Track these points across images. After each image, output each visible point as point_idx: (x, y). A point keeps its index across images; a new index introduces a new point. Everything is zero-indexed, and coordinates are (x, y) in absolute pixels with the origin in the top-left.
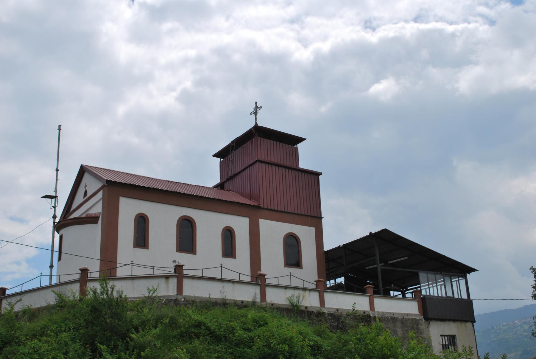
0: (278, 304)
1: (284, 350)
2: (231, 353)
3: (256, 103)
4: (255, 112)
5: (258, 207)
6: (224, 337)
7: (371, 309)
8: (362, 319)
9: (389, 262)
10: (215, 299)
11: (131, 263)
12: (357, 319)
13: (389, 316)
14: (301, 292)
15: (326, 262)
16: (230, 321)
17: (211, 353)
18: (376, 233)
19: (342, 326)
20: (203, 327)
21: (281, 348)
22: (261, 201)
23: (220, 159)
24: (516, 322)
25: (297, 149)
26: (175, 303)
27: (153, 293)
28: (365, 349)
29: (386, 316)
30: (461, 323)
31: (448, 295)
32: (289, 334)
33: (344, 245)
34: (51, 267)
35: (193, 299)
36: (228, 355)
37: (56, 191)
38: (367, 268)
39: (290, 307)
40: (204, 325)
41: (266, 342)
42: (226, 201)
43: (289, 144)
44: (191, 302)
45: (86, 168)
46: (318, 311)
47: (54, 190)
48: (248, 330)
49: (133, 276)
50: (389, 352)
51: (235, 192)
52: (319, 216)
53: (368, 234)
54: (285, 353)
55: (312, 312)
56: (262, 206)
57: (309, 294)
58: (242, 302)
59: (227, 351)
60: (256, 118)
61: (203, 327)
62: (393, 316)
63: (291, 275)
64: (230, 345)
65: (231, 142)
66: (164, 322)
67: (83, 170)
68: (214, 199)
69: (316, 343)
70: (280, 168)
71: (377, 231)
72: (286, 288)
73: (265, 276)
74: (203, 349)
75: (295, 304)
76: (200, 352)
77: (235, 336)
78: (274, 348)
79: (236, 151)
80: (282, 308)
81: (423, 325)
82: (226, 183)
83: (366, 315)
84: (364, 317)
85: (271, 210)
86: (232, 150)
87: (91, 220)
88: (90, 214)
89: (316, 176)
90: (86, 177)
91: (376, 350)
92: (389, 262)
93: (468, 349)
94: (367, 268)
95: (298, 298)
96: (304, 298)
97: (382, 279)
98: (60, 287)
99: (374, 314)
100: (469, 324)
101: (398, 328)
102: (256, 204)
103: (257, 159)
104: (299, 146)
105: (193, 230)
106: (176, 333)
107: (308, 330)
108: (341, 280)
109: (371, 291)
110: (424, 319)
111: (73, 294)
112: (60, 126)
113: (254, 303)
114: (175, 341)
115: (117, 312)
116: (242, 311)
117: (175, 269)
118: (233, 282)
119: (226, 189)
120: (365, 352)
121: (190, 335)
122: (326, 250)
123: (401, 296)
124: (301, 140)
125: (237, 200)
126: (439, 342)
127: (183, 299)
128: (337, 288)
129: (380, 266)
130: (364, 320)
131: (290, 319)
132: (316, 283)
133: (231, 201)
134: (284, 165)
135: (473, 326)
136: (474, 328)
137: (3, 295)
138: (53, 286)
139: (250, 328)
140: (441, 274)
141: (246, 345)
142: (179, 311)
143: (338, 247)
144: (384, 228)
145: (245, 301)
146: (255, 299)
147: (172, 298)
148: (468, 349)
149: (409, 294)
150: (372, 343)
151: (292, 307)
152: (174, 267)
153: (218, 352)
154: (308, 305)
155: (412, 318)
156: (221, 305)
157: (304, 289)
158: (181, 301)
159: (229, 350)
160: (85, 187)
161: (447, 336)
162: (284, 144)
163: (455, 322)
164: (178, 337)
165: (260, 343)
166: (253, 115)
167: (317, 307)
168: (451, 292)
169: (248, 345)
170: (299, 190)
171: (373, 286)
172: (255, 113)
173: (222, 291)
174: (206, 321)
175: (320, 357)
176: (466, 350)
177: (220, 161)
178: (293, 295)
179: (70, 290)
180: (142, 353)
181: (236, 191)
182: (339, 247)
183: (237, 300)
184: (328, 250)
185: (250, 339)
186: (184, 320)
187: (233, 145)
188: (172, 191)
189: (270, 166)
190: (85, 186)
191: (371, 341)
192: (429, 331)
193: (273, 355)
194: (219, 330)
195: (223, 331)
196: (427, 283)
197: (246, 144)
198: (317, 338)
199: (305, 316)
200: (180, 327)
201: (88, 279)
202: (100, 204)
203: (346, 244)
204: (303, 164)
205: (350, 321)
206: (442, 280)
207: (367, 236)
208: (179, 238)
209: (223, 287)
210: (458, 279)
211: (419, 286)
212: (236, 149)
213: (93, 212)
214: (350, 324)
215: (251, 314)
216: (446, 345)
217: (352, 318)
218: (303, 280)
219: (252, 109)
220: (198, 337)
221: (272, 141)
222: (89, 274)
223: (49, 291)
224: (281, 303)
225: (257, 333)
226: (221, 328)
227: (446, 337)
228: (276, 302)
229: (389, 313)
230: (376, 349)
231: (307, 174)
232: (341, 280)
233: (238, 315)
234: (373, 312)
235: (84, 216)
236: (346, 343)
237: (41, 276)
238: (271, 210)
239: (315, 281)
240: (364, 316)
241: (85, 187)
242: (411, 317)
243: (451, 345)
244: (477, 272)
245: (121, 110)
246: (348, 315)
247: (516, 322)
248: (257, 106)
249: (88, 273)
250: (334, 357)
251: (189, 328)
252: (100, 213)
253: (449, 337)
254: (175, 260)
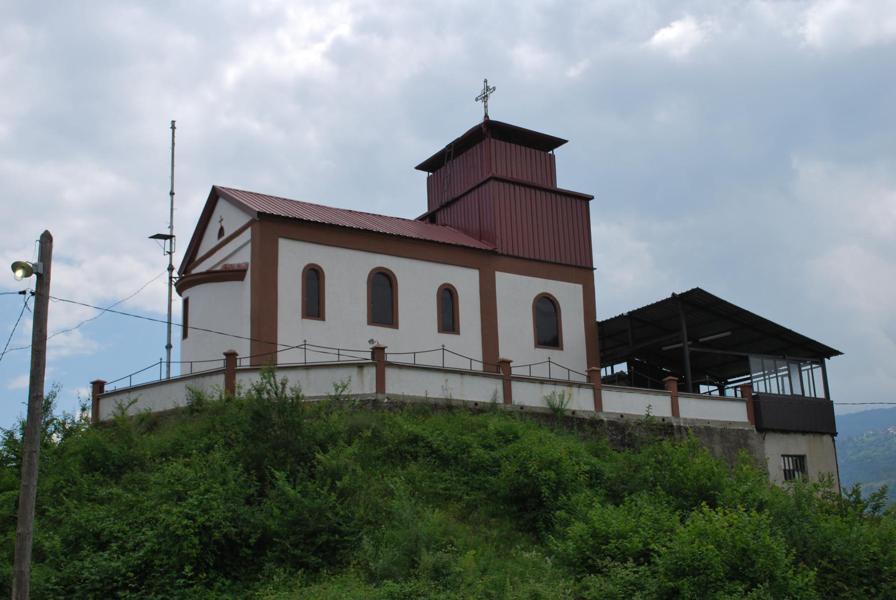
0: (530, 407)
1: (549, 479)
2: (466, 483)
3: (486, 81)
4: (483, 96)
5: (494, 253)
6: (453, 458)
7: (673, 415)
8: (661, 430)
9: (701, 340)
10: (434, 399)
11: (304, 343)
12: (652, 430)
13: (702, 426)
14: (566, 389)
15: (600, 339)
16: (462, 434)
17: (435, 482)
18: (682, 295)
19: (628, 441)
20: (422, 442)
21: (545, 476)
22: (498, 242)
23: (427, 173)
24: (889, 429)
25: (552, 158)
26: (374, 405)
27: (342, 391)
28: (671, 477)
29: (697, 425)
30: (814, 436)
31: (794, 393)
32: (557, 455)
33: (629, 313)
34: (169, 347)
35: (401, 399)
36: (461, 486)
37: (171, 227)
38: (664, 349)
39: (550, 412)
40: (422, 441)
41: (520, 466)
42: (444, 243)
43: (540, 149)
44: (399, 405)
45: (221, 191)
46: (592, 417)
47: (169, 225)
48: (489, 447)
49: (307, 364)
50: (708, 482)
51: (454, 227)
52: (588, 266)
53: (669, 296)
54: (551, 483)
55: (584, 419)
56: (499, 250)
57: (579, 391)
58: (476, 404)
59: (459, 481)
60: (486, 107)
61: (421, 444)
62: (708, 425)
63: (549, 361)
64: (463, 470)
65: (447, 146)
66: (365, 436)
67: (216, 195)
68: (418, 239)
69: (594, 468)
70: (528, 190)
71: (684, 291)
72: (542, 381)
73: (511, 363)
74: (423, 476)
75: (556, 406)
76: (419, 482)
77: (471, 457)
78: (534, 475)
79: (454, 161)
80: (537, 413)
81: (755, 438)
82: (439, 213)
83: (666, 424)
84: (662, 428)
85: (514, 257)
86: (448, 159)
87: (233, 274)
88: (231, 265)
89: (584, 202)
90: (222, 205)
91: (688, 479)
92: (701, 340)
93: (826, 478)
94: (664, 349)
95: (562, 397)
96: (570, 398)
97: (692, 369)
98: (194, 380)
99: (679, 422)
100: (827, 439)
101: (715, 444)
102: (490, 248)
103: (490, 175)
104: (558, 152)
105: (392, 290)
106: (381, 453)
107: (581, 447)
108: (622, 368)
109: (674, 385)
110: (757, 430)
111: (219, 393)
112: (173, 122)
113: (493, 406)
114: (380, 464)
115: (293, 421)
116: (480, 418)
117: (373, 353)
118: (462, 373)
119: (440, 223)
120: (671, 481)
121: (401, 454)
122: (600, 321)
123: (717, 393)
124: (559, 142)
125: (460, 243)
126: (780, 466)
127: (386, 400)
128: (615, 381)
129: (687, 347)
130: (663, 431)
131: (552, 430)
132: (588, 374)
133: (452, 243)
134: (533, 185)
135: (834, 441)
136: (834, 444)
137: (101, 393)
138: (173, 380)
139: (492, 444)
140: (784, 358)
141: (488, 470)
142: (383, 419)
143: (620, 315)
144: (696, 287)
145: (480, 402)
146: (496, 399)
147: (369, 398)
148: (826, 478)
149: (731, 389)
150: (682, 468)
151: (552, 412)
152: (371, 350)
153: (446, 480)
154: (577, 409)
156: (443, 409)
157: (570, 384)
158: (383, 402)
159: (463, 479)
160: (220, 221)
161: (792, 456)
162: (533, 150)
163: (804, 435)
164: (384, 457)
165: (509, 468)
166: (481, 101)
167: (590, 411)
168: (800, 388)
169: (491, 471)
170: (558, 224)
171: (677, 379)
172: (485, 98)
173: (445, 387)
174: (426, 434)
175: (600, 489)
176: (824, 479)
177: (427, 176)
178: (554, 393)
179: (215, 387)
180: (337, 482)
181: (456, 225)
182: (622, 316)
183: (468, 401)
184: (604, 320)
185: (494, 462)
186: (391, 432)
187: (451, 151)
188: (359, 228)
189: (512, 186)
190: (220, 219)
191: (680, 464)
192: (764, 449)
193: (532, 486)
194: (446, 448)
195: (452, 450)
196: (762, 373)
197: (471, 150)
198: (594, 460)
199: (572, 426)
200: (386, 444)
201: (238, 368)
202: (248, 249)
203: (634, 312)
204: (563, 183)
205: (642, 434)
206: (783, 368)
207: (667, 300)
208: (372, 303)
209: (447, 380)
210: (811, 366)
211: (749, 376)
212: (455, 156)
213: (235, 261)
214: (642, 438)
215: (494, 423)
216: (789, 470)
217: (644, 429)
218: (569, 370)
219: (479, 90)
220: (415, 458)
221: (513, 145)
222: (238, 361)
223: (181, 385)
224: (535, 406)
225: (505, 453)
226: (448, 445)
227: (790, 459)
228: (527, 404)
229: (702, 420)
230: (689, 477)
231: (570, 199)
232: (622, 368)
233: (473, 424)
234: (677, 420)
235: (219, 268)
236: (638, 468)
237: (161, 362)
238: (514, 257)
240: (664, 426)
241: (220, 221)
242: (736, 428)
243: (798, 471)
244: (842, 355)
245: (231, 74)
246: (639, 424)
247: (889, 429)
248: (487, 87)
249: (237, 359)
250: (622, 488)
251: (400, 444)
252: (247, 264)
253: (795, 458)
254: (372, 339)
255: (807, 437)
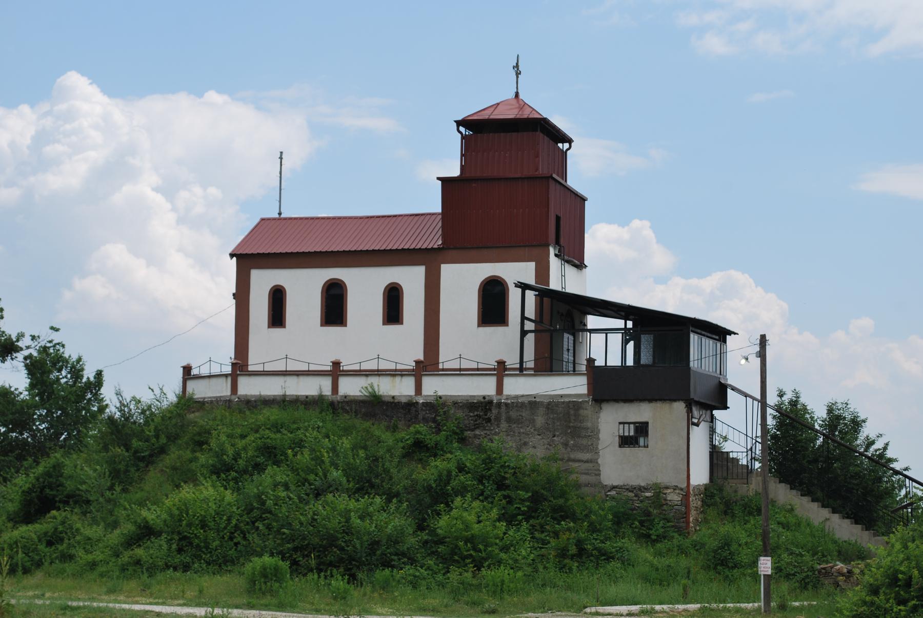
10: (274, 396)
13: (526, 400)
95: (372, 386)
155: (570, 401)
192: (598, 418)
209: (285, 382)
239: (496, 362)
242: (567, 400)
255: (653, 405)
